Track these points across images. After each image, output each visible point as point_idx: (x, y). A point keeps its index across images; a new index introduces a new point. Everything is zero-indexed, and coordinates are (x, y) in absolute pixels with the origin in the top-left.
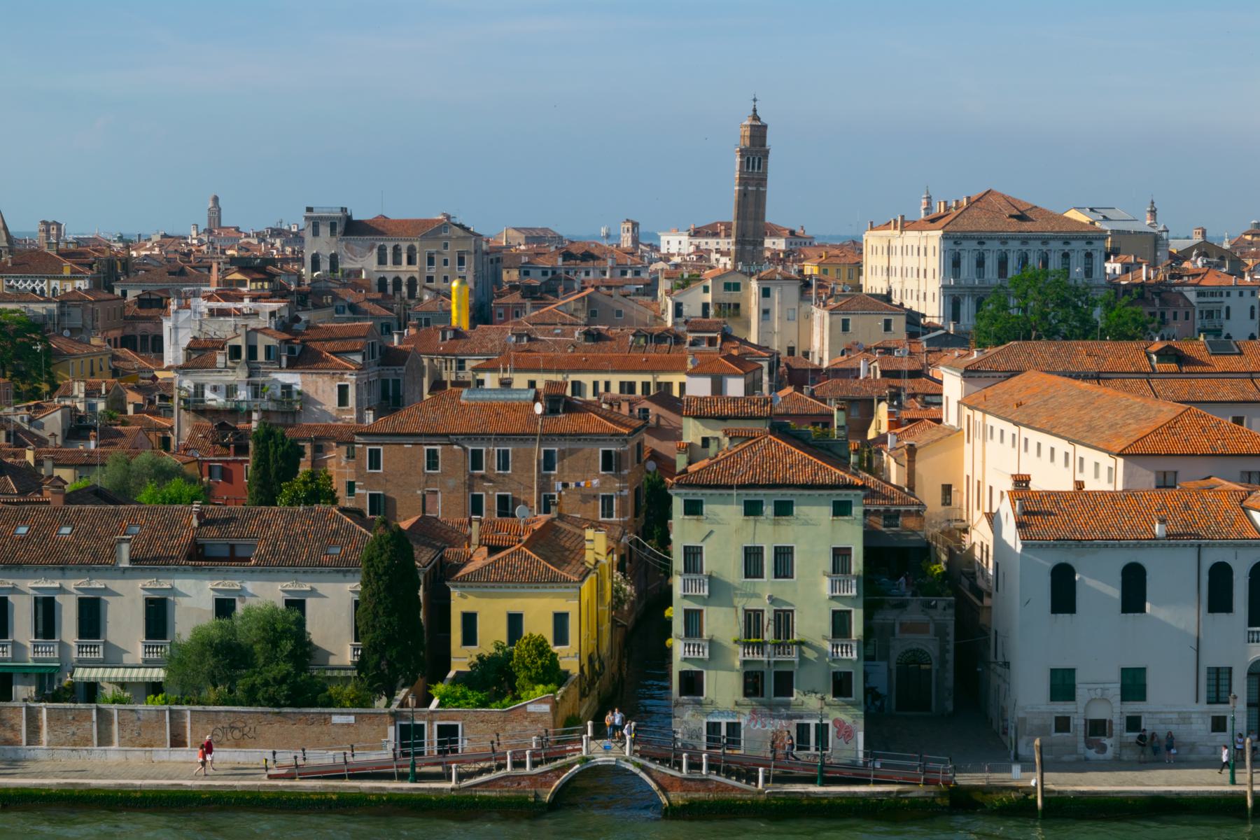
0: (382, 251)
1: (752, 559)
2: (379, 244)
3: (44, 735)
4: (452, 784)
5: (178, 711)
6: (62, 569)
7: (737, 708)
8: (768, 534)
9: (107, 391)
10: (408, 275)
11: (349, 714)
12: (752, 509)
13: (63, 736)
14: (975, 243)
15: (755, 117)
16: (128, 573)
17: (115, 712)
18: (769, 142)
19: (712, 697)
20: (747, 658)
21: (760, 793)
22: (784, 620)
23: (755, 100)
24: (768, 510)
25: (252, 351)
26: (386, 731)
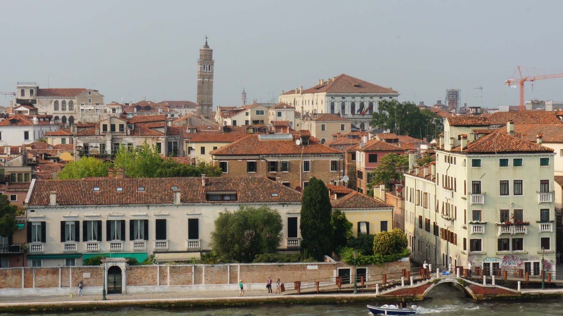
0: (56, 103)
1: (504, 185)
2: (55, 100)
3: (168, 280)
4: (377, 293)
5: (233, 266)
6: (148, 206)
7: (497, 256)
8: (510, 174)
9: (22, 151)
10: (70, 115)
11: (315, 265)
12: (504, 163)
13: (177, 280)
14: (340, 98)
15: (207, 46)
16: (180, 207)
17: (204, 267)
18: (213, 59)
19: (485, 251)
20: (503, 232)
21: (519, 293)
22: (518, 214)
23: (206, 38)
24: (511, 162)
25: (113, 127)
26: (332, 272)
